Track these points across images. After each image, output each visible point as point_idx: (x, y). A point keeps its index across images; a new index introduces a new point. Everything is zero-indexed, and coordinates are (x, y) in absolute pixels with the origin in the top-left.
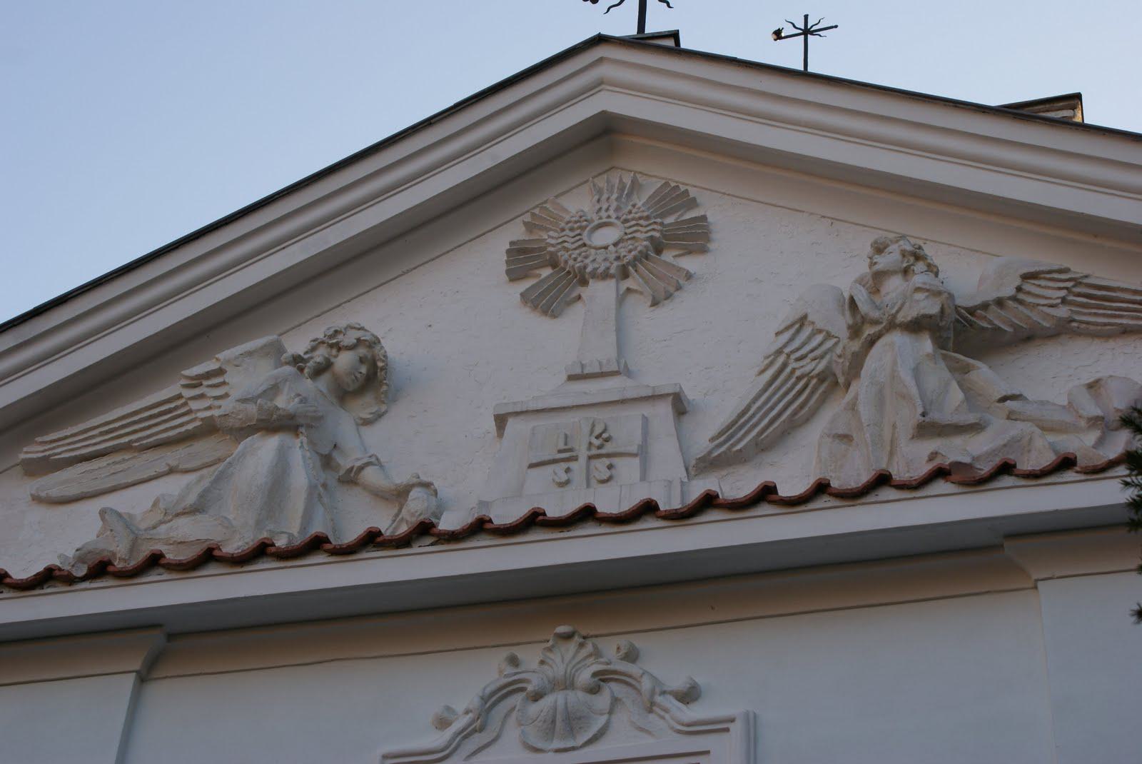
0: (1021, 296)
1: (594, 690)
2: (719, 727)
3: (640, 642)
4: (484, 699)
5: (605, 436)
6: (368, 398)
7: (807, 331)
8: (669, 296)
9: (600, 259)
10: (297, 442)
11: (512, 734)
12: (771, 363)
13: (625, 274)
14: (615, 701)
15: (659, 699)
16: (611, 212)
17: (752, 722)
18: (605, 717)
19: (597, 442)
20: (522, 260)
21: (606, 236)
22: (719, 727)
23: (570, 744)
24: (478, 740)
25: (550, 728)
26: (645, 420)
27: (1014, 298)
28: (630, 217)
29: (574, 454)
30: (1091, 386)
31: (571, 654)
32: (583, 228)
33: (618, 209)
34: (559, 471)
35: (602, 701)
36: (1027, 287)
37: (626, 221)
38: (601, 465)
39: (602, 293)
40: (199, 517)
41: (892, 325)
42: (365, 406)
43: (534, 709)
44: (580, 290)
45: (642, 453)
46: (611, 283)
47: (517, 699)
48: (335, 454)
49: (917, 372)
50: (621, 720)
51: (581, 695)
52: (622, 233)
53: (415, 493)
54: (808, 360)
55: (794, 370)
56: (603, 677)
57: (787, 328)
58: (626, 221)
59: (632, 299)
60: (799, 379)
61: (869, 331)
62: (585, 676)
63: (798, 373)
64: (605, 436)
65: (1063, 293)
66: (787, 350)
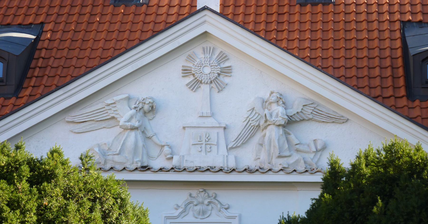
0: (303, 111)
1: (208, 205)
2: (234, 218)
3: (217, 192)
4: (185, 205)
5: (209, 138)
6: (151, 113)
7: (254, 112)
8: (222, 90)
9: (206, 78)
10: (138, 132)
11: (191, 213)
12: (246, 120)
13: (211, 82)
14: (212, 208)
15: (221, 210)
16: (208, 62)
17: (240, 216)
18: (210, 212)
19: (207, 140)
20: (186, 72)
21: (207, 70)
22: (234, 218)
23: (203, 217)
24: (184, 214)
25: (199, 213)
26: (218, 133)
27: (301, 112)
28: (213, 65)
29: (194, 90)
30: (314, 140)
31: (202, 196)
32: (201, 66)
33: (209, 61)
34: (199, 146)
35: (210, 207)
36: (304, 109)
37: (212, 66)
38: (208, 147)
39: (205, 88)
40: (120, 156)
41: (274, 124)
42: (150, 116)
43: (196, 208)
44: (201, 85)
45: (218, 144)
46: (208, 85)
47: (191, 205)
48: (145, 131)
49: (279, 140)
50: (214, 212)
51: (205, 206)
52: (210, 71)
53: (166, 147)
54: (254, 121)
55: (251, 124)
56: (210, 203)
57: (250, 110)
58: (212, 66)
59: (213, 89)
60: (252, 126)
61: (268, 123)
62: (206, 202)
63: (252, 125)
64: (209, 138)
65: (311, 111)
66: (250, 117)
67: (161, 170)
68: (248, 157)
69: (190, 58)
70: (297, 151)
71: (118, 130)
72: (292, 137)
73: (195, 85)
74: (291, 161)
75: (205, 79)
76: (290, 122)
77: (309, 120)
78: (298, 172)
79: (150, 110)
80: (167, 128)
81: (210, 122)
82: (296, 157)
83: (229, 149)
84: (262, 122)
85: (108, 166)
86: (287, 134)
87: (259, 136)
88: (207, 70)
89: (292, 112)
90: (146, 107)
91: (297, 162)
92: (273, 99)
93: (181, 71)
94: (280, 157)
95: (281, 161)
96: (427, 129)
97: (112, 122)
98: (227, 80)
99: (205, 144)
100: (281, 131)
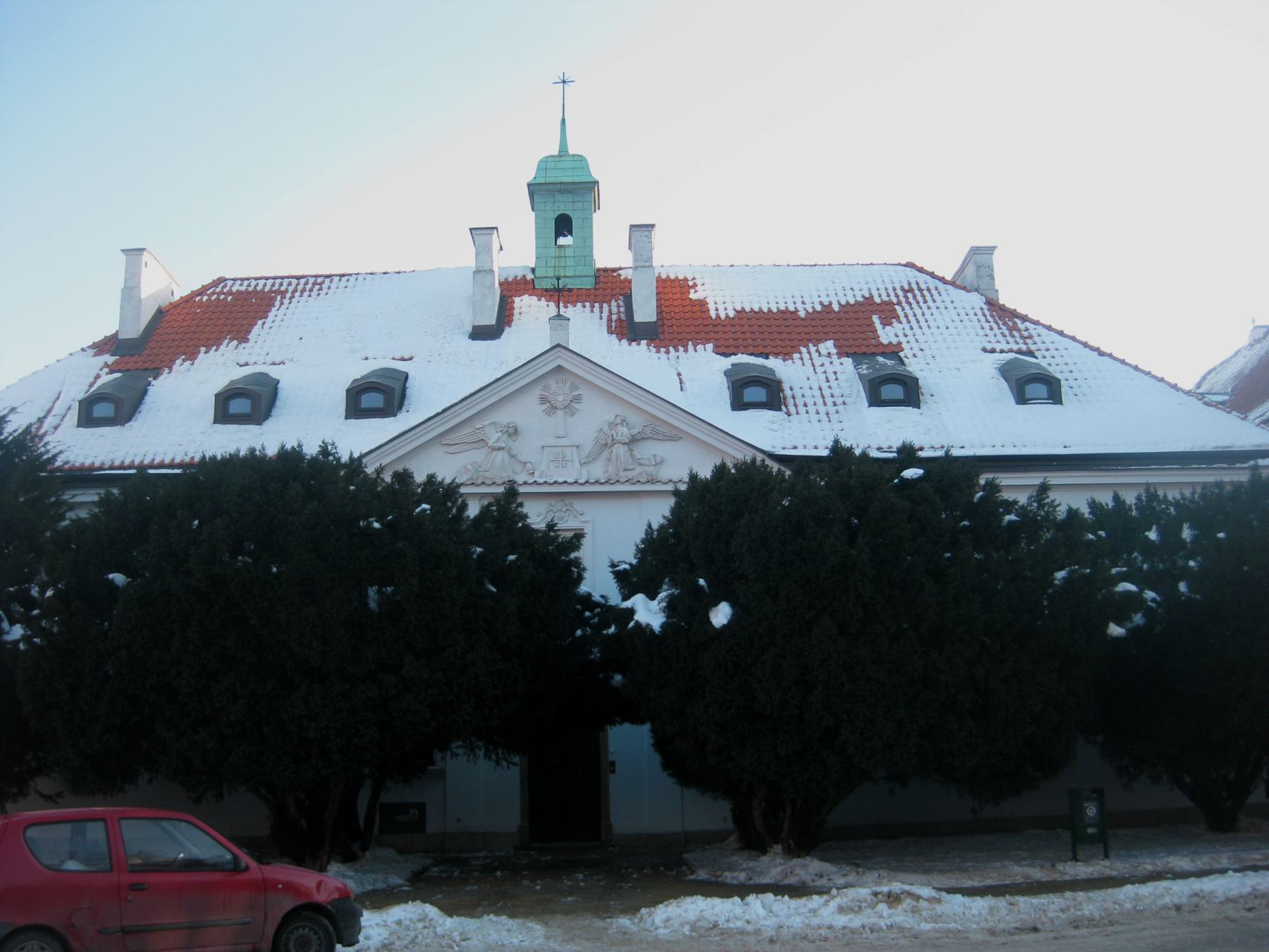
20: (543, 400)
21: (561, 398)
39: (560, 413)
67: (525, 483)
68: (597, 471)
69: (546, 388)
70: (640, 464)
71: (486, 450)
72: (635, 453)
73: (553, 409)
74: (635, 473)
75: (559, 405)
76: (633, 440)
77: (649, 438)
78: (1007, 344)
79: (513, 432)
80: (526, 448)
81: (563, 442)
82: (639, 469)
83: (581, 465)
84: (609, 441)
85: (479, 482)
86: (631, 450)
87: (606, 453)
88: (561, 398)
89: (634, 432)
90: (511, 430)
91: (640, 474)
92: (618, 421)
93: (794, 417)
94: (626, 470)
95: (626, 473)
96: (292, 635)
97: (481, 444)
98: (577, 406)
99: (562, 462)
100: (626, 448)
